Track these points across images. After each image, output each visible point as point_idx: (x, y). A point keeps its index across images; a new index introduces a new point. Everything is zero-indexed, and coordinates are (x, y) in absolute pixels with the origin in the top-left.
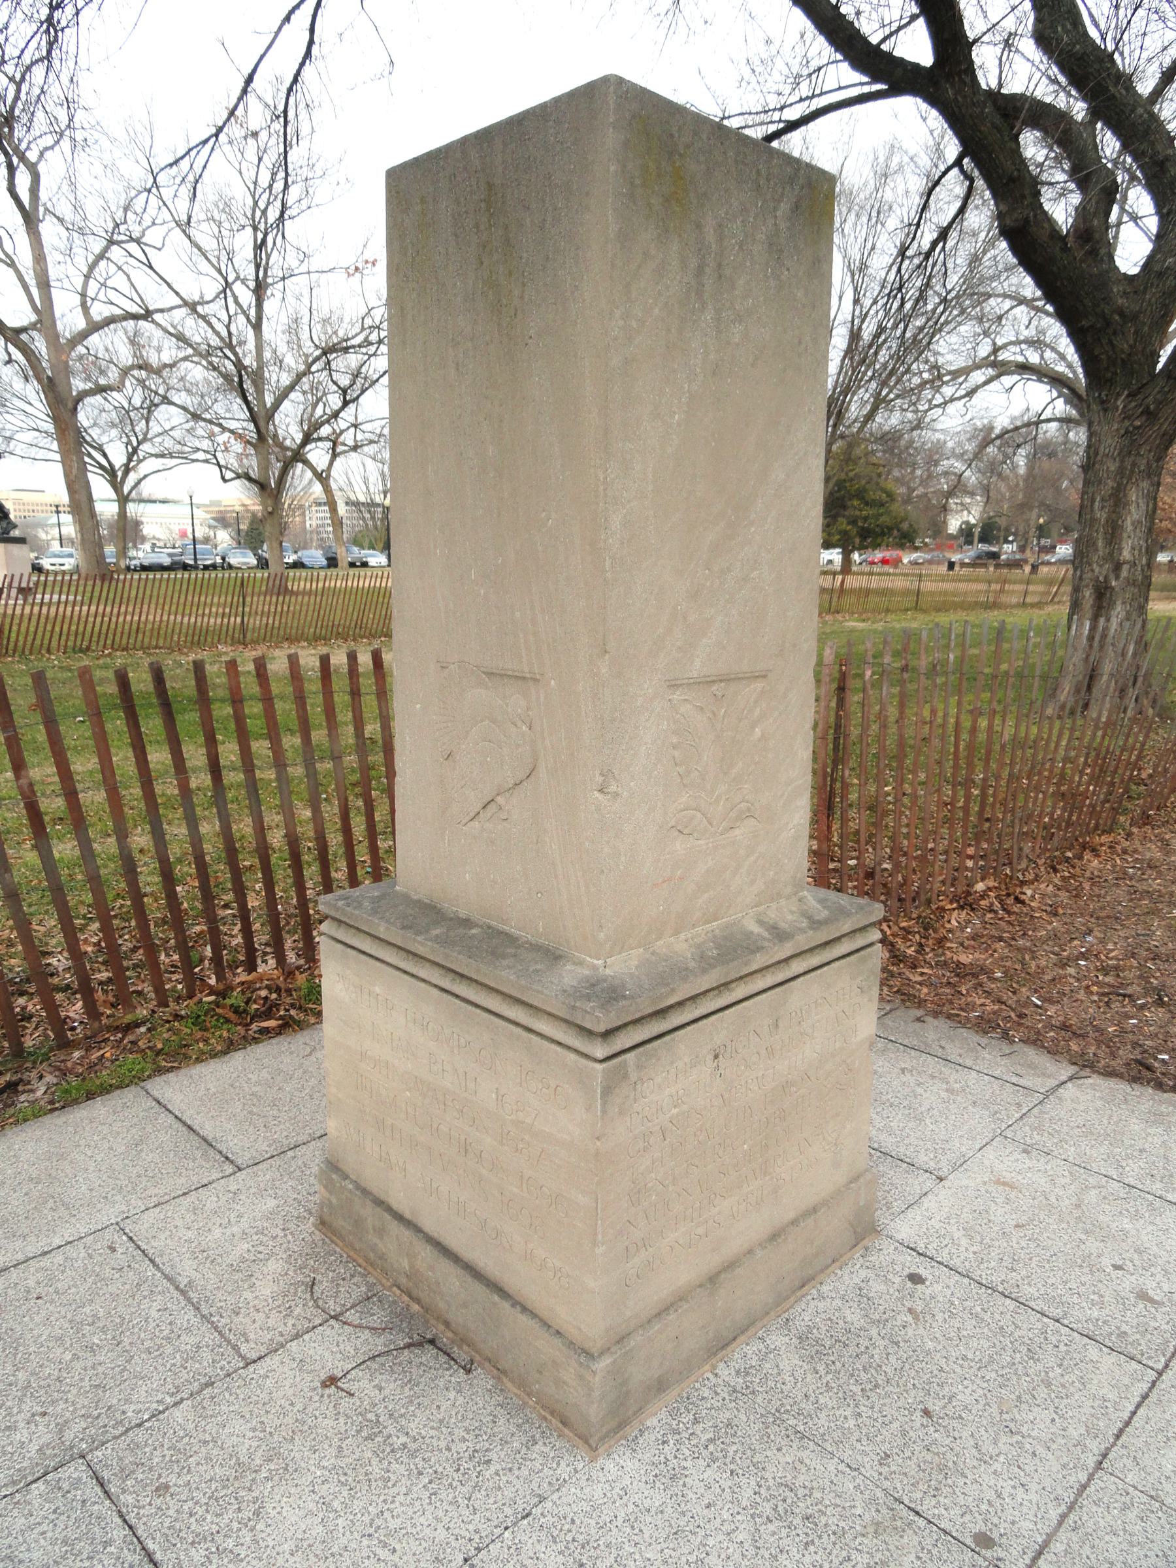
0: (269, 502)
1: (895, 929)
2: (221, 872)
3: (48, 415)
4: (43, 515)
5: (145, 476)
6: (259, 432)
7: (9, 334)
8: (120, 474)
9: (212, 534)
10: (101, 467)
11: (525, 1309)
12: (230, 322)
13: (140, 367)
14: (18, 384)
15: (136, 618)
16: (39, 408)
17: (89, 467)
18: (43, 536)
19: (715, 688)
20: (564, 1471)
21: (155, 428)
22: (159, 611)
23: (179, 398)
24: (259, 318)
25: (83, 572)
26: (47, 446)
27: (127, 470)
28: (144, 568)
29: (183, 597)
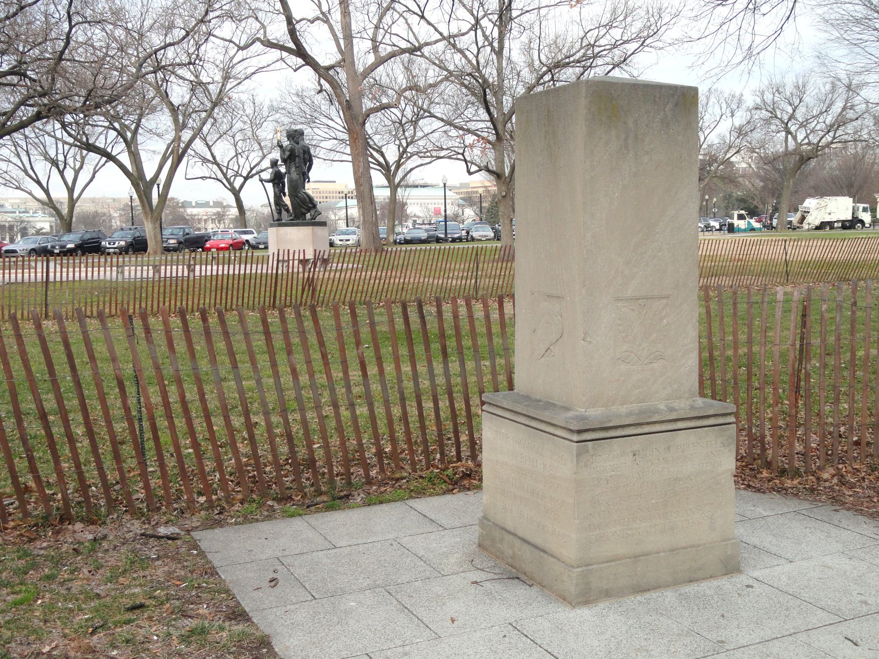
0: (504, 188)
1: (849, 468)
2: (449, 425)
3: (344, 128)
4: (333, 200)
5: (412, 170)
6: (497, 134)
7: (322, 71)
8: (393, 168)
9: (460, 211)
10: (379, 164)
11: (552, 556)
12: (478, 53)
13: (410, 89)
14: (325, 106)
15: (402, 280)
16: (338, 121)
17: (372, 165)
18: (333, 217)
19: (640, 301)
20: (560, 610)
21: (419, 134)
22: (418, 275)
23: (437, 110)
24: (501, 47)
25: (363, 247)
26: (341, 150)
27: (399, 165)
28: (407, 242)
29: (435, 264)
